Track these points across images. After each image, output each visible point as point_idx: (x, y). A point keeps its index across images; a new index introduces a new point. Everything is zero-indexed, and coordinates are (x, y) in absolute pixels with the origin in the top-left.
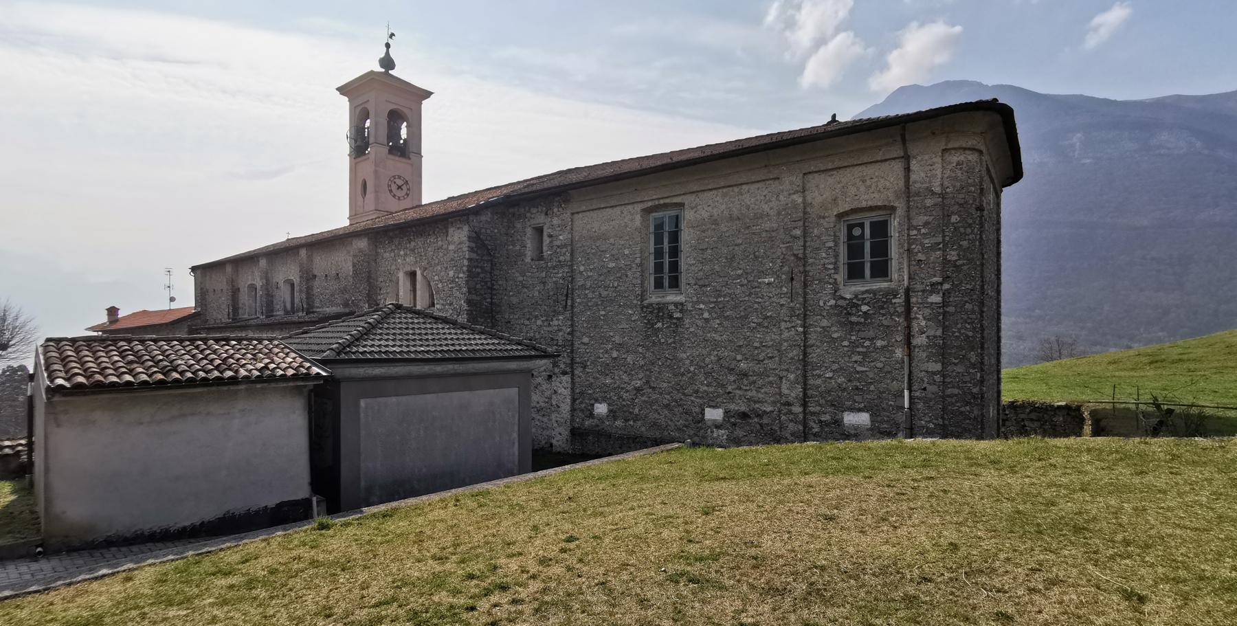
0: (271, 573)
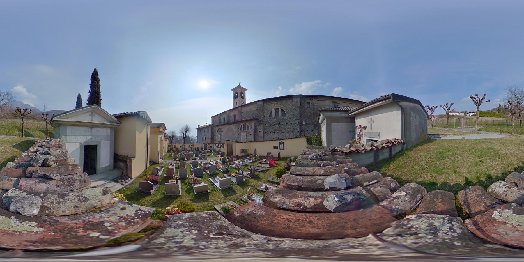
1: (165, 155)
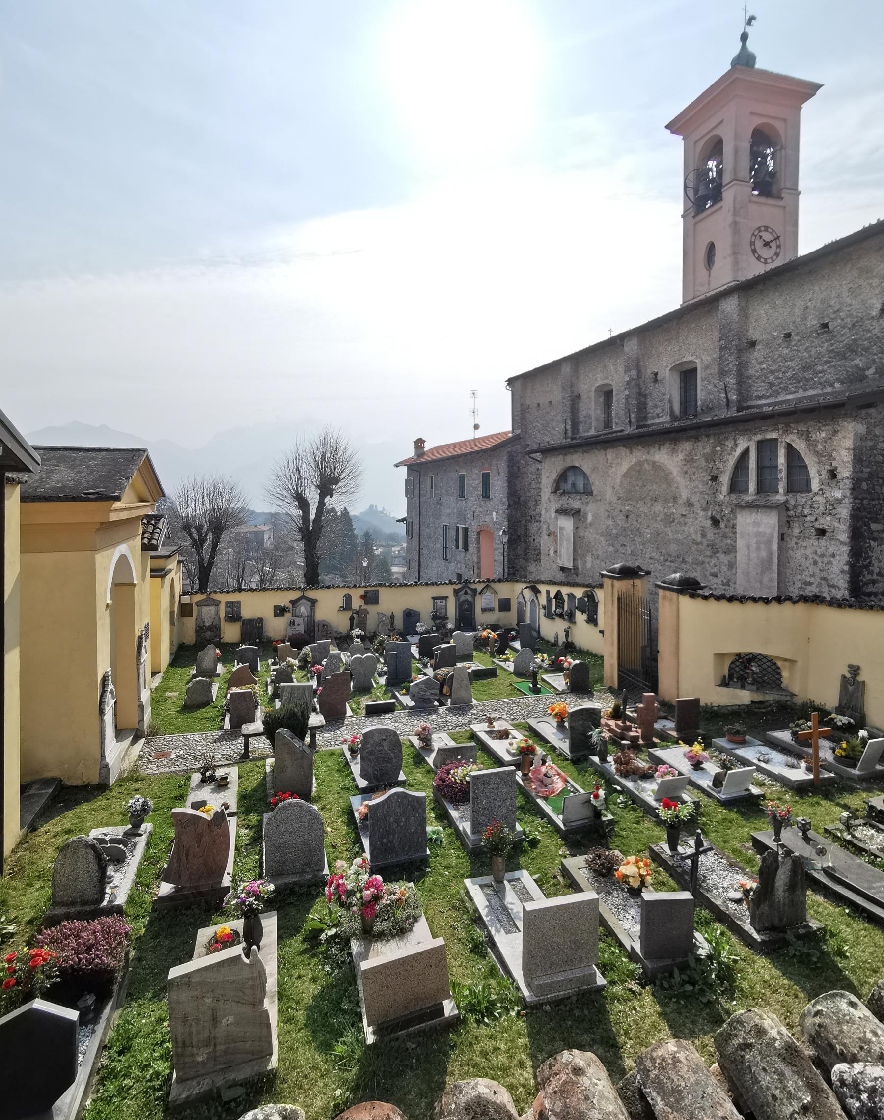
0: (424, 730)
1: (158, 700)
